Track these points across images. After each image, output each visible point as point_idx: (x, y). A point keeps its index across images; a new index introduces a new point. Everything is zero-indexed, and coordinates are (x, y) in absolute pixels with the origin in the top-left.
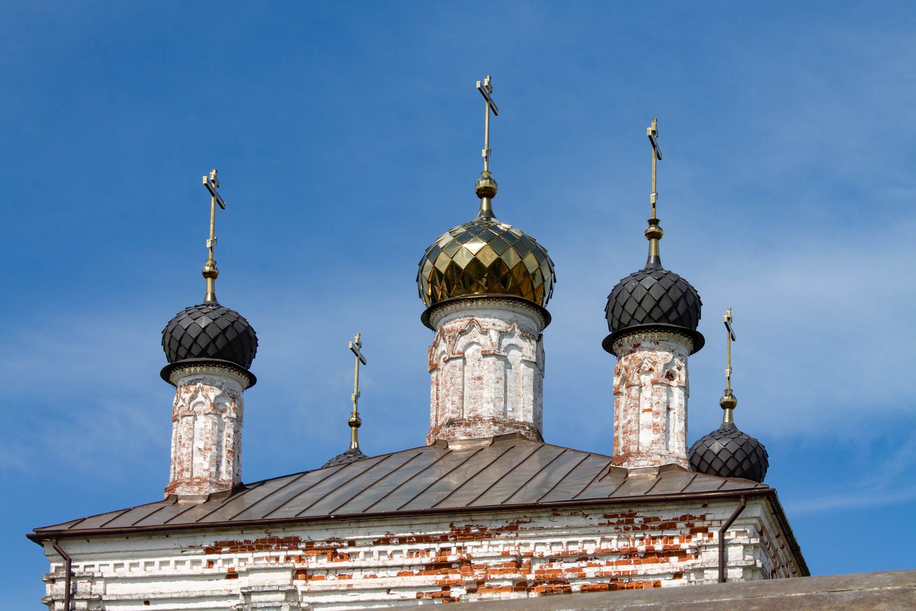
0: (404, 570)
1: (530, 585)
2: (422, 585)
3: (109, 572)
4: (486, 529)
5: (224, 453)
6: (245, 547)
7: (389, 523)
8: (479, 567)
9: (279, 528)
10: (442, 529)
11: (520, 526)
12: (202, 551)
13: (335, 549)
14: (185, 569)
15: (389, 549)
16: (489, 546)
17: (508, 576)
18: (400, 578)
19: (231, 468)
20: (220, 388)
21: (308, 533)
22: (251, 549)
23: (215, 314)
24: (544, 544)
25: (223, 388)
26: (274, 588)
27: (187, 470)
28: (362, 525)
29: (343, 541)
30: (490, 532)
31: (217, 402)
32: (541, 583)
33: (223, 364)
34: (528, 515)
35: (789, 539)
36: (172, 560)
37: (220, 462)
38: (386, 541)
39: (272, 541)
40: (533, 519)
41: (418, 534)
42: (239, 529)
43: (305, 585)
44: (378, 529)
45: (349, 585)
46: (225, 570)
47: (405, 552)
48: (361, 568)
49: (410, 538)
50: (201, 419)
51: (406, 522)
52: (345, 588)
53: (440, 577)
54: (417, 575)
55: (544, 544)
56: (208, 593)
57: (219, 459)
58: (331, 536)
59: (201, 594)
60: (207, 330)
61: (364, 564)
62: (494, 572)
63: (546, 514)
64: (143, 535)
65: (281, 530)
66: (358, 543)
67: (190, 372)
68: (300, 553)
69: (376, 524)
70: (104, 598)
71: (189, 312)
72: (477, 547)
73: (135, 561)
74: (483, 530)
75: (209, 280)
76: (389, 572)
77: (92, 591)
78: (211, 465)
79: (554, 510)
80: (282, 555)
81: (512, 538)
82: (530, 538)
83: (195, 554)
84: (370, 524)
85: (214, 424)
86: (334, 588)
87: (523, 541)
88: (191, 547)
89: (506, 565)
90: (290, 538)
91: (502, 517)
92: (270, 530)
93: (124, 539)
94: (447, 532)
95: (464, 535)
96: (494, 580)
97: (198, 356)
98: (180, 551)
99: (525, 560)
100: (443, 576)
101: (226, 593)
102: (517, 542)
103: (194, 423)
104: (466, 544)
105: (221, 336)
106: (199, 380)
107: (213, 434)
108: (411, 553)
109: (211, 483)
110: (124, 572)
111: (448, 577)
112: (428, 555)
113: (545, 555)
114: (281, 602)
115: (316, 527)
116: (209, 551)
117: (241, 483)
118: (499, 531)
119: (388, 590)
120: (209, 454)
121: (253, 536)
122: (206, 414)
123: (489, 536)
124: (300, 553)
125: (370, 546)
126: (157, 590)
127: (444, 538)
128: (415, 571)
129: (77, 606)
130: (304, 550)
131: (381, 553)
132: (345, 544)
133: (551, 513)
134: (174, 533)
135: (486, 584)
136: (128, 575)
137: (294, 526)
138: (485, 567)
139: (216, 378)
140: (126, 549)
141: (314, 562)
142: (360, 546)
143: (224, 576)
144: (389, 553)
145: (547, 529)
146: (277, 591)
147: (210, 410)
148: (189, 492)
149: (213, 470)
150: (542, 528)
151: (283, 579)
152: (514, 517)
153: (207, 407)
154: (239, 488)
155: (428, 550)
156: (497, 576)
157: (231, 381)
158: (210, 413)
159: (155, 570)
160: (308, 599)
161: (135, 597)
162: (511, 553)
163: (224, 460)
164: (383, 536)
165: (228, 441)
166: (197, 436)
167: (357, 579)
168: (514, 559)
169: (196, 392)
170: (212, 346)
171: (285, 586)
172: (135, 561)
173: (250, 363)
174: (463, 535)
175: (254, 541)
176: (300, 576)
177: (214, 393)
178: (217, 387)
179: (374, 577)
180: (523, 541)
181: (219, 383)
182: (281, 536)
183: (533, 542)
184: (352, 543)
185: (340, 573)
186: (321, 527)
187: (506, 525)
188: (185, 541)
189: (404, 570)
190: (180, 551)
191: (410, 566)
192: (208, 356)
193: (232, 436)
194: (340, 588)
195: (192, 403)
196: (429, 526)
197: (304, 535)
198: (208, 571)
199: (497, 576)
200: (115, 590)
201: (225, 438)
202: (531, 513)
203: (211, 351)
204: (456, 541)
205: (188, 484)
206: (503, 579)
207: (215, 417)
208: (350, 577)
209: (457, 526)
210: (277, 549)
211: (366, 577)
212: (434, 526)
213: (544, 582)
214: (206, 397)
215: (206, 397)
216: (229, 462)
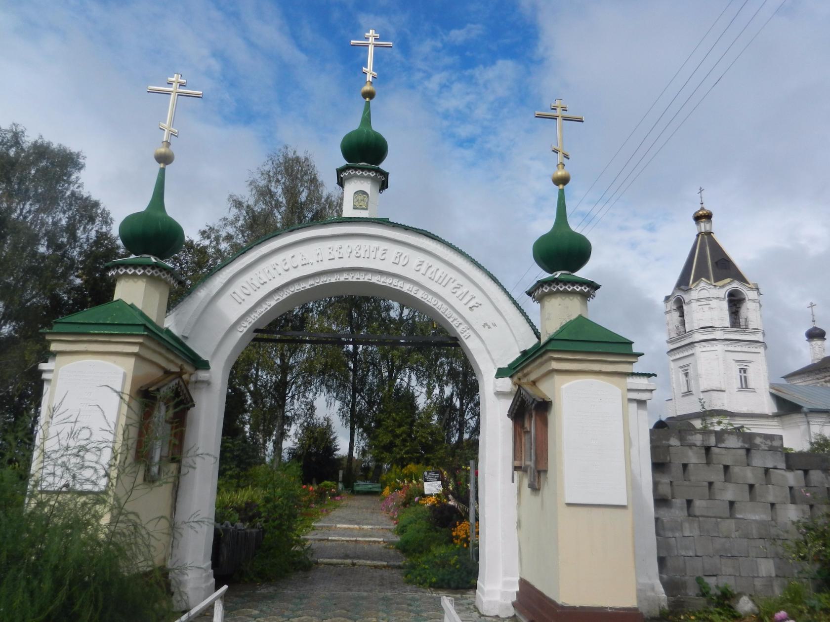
72: (744, 385)
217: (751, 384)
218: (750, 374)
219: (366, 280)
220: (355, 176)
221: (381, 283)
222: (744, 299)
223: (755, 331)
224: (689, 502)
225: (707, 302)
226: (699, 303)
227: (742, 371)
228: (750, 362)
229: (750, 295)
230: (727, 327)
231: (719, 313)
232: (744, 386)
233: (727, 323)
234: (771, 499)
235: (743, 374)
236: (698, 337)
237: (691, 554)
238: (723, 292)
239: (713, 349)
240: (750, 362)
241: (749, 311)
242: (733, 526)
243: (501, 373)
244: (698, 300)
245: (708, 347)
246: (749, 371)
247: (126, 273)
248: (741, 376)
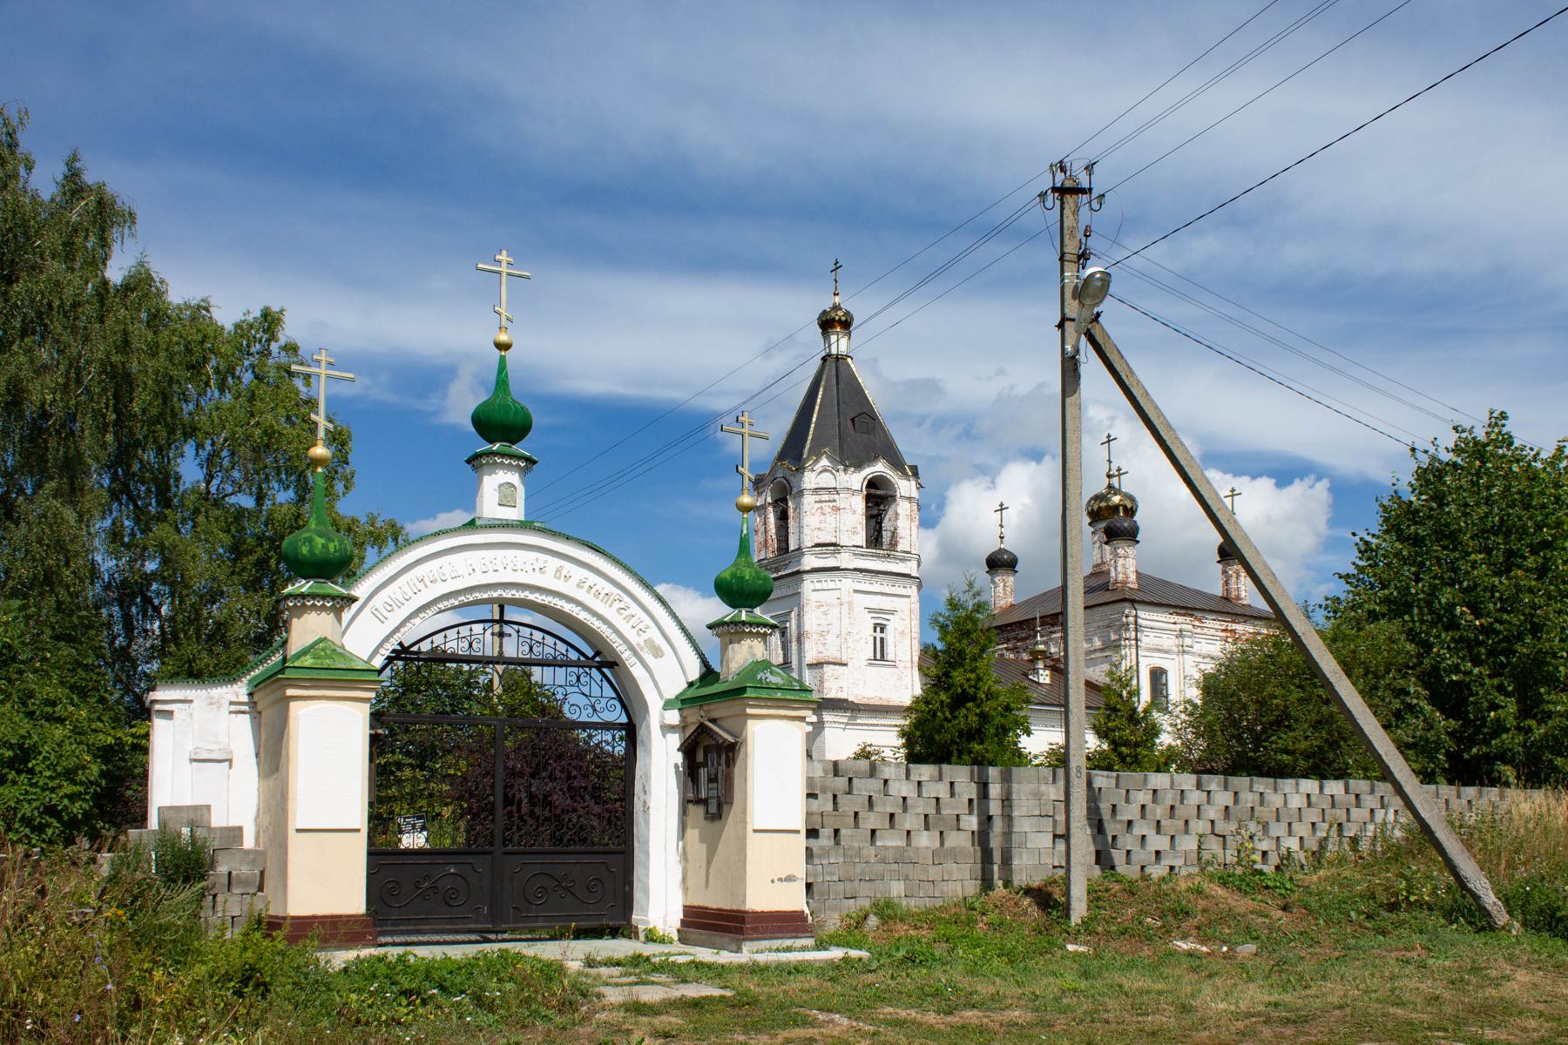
0: (1217, 630)
72: (880, 654)
121: (1183, 611)
141: (1197, 623)
167: (1205, 630)
174: (1233, 622)
185: (1202, 628)
189: (1217, 630)
197: (1196, 614)
217: (890, 655)
218: (890, 636)
219: (522, 596)
220: (502, 465)
221: (539, 601)
222: (893, 497)
223: (906, 557)
224: (836, 832)
225: (832, 497)
226: (818, 498)
227: (878, 629)
228: (892, 612)
229: (905, 487)
230: (862, 547)
231: (851, 520)
232: (878, 657)
233: (861, 539)
234: (908, 827)
235: (879, 635)
236: (809, 562)
237: (835, 878)
238: (856, 479)
239: (831, 585)
240: (892, 612)
241: (903, 518)
242: (873, 852)
243: (668, 705)
244: (816, 490)
245: (826, 581)
246: (889, 629)
247: (314, 605)
248: (875, 638)
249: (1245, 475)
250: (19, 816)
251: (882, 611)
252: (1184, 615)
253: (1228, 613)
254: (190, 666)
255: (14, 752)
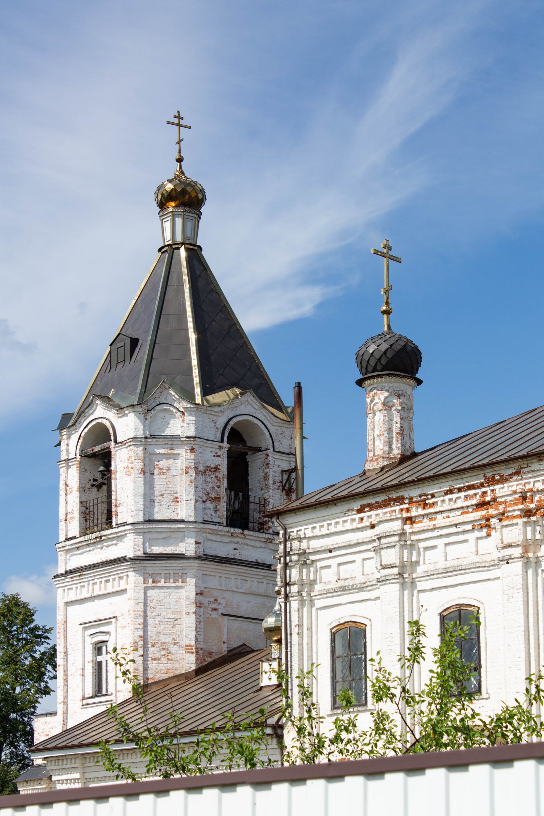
0: (464, 510)
1: (534, 511)
2: (473, 519)
3: (309, 533)
4: (503, 475)
5: (395, 435)
6: (376, 506)
7: (450, 479)
8: (501, 503)
9: (392, 491)
10: (480, 479)
11: (523, 470)
12: (354, 512)
13: (424, 500)
14: (348, 526)
15: (454, 496)
16: (509, 486)
17: (516, 507)
18: (462, 516)
19: (399, 445)
20: (388, 391)
21: (409, 492)
22: (380, 507)
23: (392, 341)
24: (539, 481)
25: (390, 391)
26: (392, 533)
27: (371, 451)
28: (436, 482)
29: (428, 495)
30: (507, 477)
31: (386, 401)
32: (540, 509)
33: (387, 375)
34: (525, 462)
35: (301, 664)
36: (341, 520)
37: (392, 441)
38: (450, 492)
39: (391, 500)
40: (529, 465)
41: (467, 484)
42: (371, 495)
43: (411, 528)
44: (445, 484)
45: (434, 525)
46: (368, 524)
47: (463, 497)
48: (441, 512)
49: (463, 487)
50: (378, 413)
51: (459, 477)
52: (431, 527)
53: (484, 513)
54: (471, 512)
55: (539, 481)
56: (360, 541)
57: (391, 440)
58: (420, 493)
59: (356, 542)
60: (374, 354)
61: (441, 509)
62: (510, 506)
63: (535, 461)
64: (323, 506)
65: (393, 492)
66: (436, 495)
67: (370, 382)
68: (406, 506)
69: (443, 481)
70: (308, 551)
71: (373, 341)
72: (502, 488)
73: (322, 524)
74: (502, 476)
75: (385, 316)
76: (456, 512)
77: (301, 548)
78: (384, 446)
79: (539, 457)
80: (397, 508)
81: (520, 480)
82: (530, 478)
83: (352, 515)
84: (440, 481)
85: (385, 416)
86: (426, 528)
87: (527, 481)
88: (349, 510)
89: (517, 499)
90: (399, 497)
91: (511, 466)
92: (388, 493)
93: (314, 510)
94: (482, 481)
95: (493, 482)
96: (509, 511)
97: (381, 371)
98: (343, 514)
99: (529, 494)
100: (486, 511)
101: (369, 539)
102: (524, 482)
103: (374, 418)
104: (496, 487)
105: (384, 356)
106: (374, 389)
107: (384, 424)
108: (466, 497)
109: (384, 458)
110: (317, 532)
111: (488, 512)
112: (476, 498)
113: (540, 489)
114: (395, 542)
115: (412, 488)
116: (359, 511)
117: (414, 452)
118: (511, 476)
119: (456, 525)
120: (382, 438)
121: (380, 498)
122: (380, 411)
123: (506, 480)
124: (406, 506)
125: (443, 496)
126: (335, 542)
127: (482, 485)
128: (471, 510)
129: (292, 559)
130: (409, 504)
131: (450, 500)
132: (429, 497)
133: (538, 459)
134: (339, 502)
135: (506, 514)
136: (319, 533)
137: (400, 488)
138: (505, 503)
139: (385, 385)
140: (316, 517)
141: (415, 512)
142: (438, 497)
143: (369, 528)
144: (454, 499)
145: (538, 470)
146: (394, 535)
147: (381, 408)
148: (372, 466)
149: (386, 448)
150: (534, 471)
151: (397, 525)
152: (517, 465)
153: (380, 406)
154: (404, 459)
155: (476, 494)
156: (510, 509)
157: (396, 384)
158: (381, 410)
159: (332, 529)
160: (414, 538)
161: (323, 549)
162: (518, 491)
163: (395, 440)
164: (448, 488)
165: (396, 427)
166: (376, 426)
167: (440, 520)
168: (521, 495)
169: (373, 396)
170: (379, 363)
171: (397, 531)
172: (322, 524)
173: (417, 370)
174: (492, 481)
175: (380, 501)
176: (408, 522)
177: (382, 396)
178: (385, 391)
179: (448, 517)
180: (527, 481)
181: (387, 388)
182: (394, 496)
183: (532, 480)
184: (433, 496)
185: (430, 517)
186: (414, 487)
187: (514, 471)
188: (344, 507)
189: (464, 510)
190: (343, 514)
191: (467, 507)
192: (378, 371)
193: (399, 422)
194: (430, 528)
195: (372, 404)
196: (473, 478)
197: (407, 493)
198: (360, 525)
199: (510, 509)
200: (315, 544)
201: (394, 424)
202: (526, 461)
203: (379, 367)
204: (489, 486)
205: (371, 461)
206: (514, 510)
207: (385, 412)
208: (435, 519)
209: (488, 475)
210: (394, 505)
211: (444, 518)
212: (475, 477)
213: (542, 508)
214: (379, 399)
215: (379, 399)
216: (397, 441)
240: (107, 621)
249: (243, 783)
250: (352, 731)
251: (100, 622)
252: (385, 504)
253: (472, 468)
254: (407, 659)
255: (187, 775)
